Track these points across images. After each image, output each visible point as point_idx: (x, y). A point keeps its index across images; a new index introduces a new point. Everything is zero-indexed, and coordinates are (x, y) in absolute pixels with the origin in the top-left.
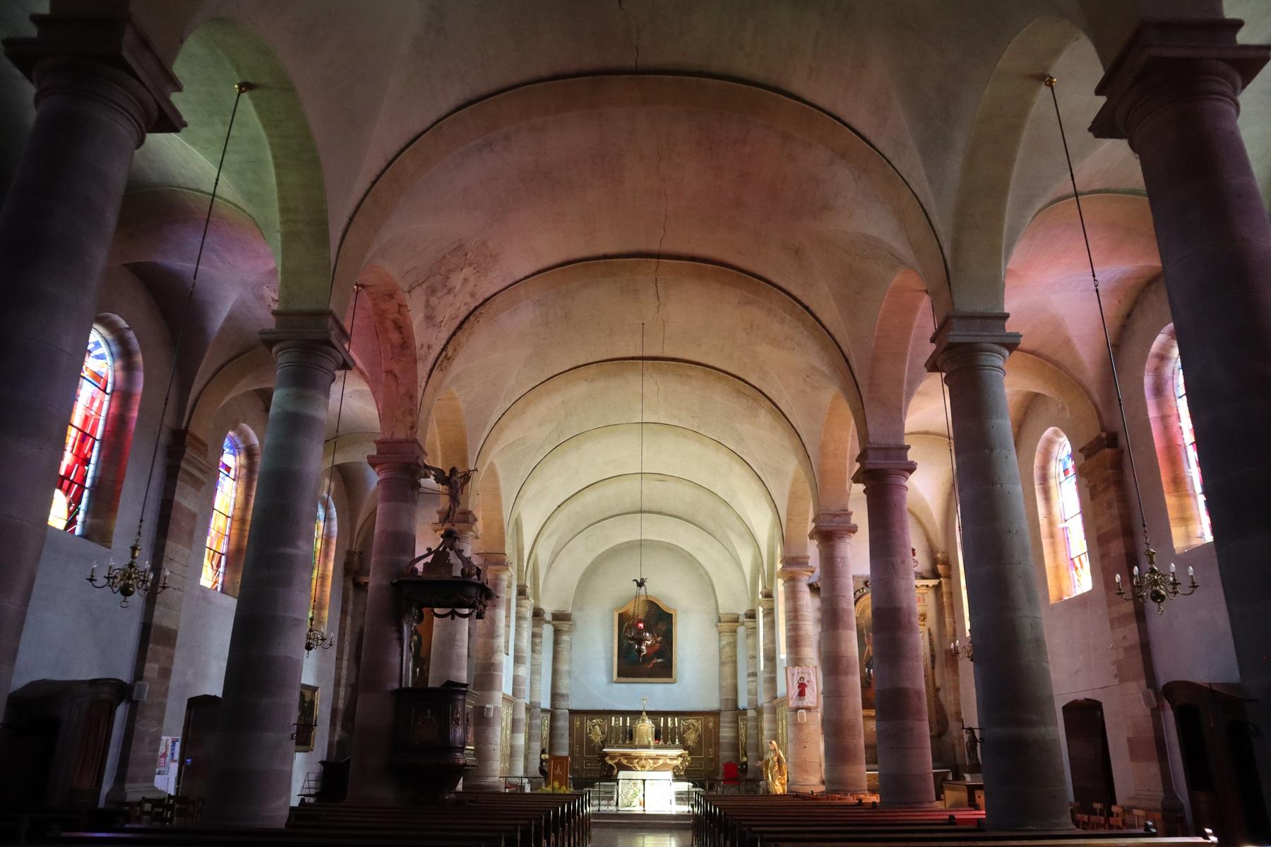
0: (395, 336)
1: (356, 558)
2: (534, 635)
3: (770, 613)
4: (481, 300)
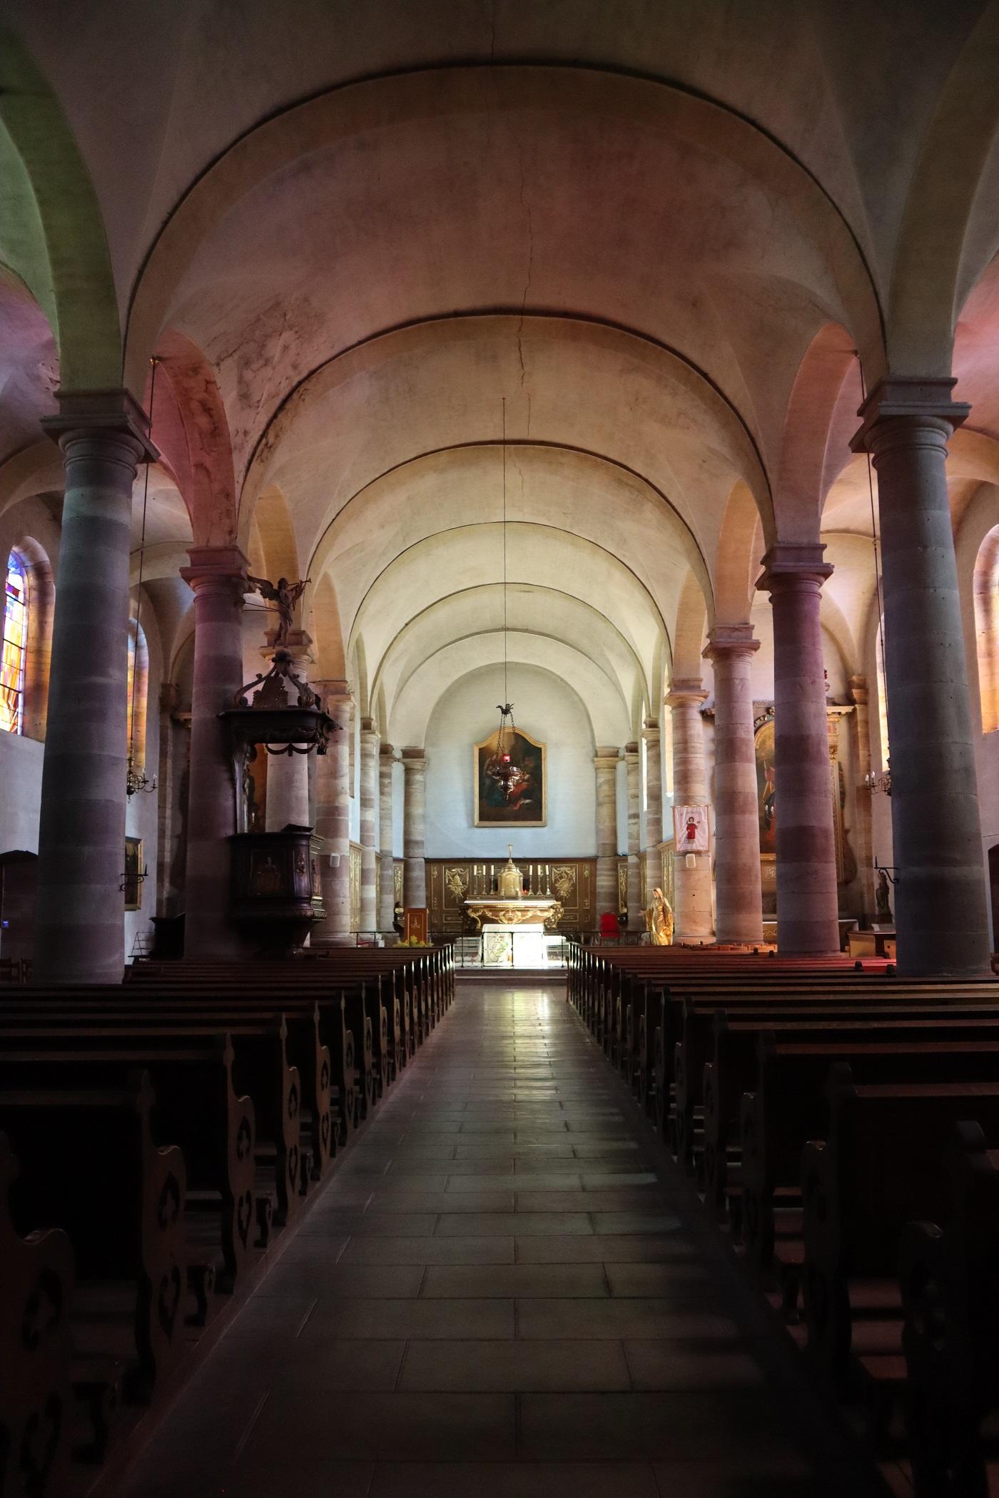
0: (203, 421)
1: (173, 692)
2: (382, 775)
3: (655, 745)
4: (305, 374)
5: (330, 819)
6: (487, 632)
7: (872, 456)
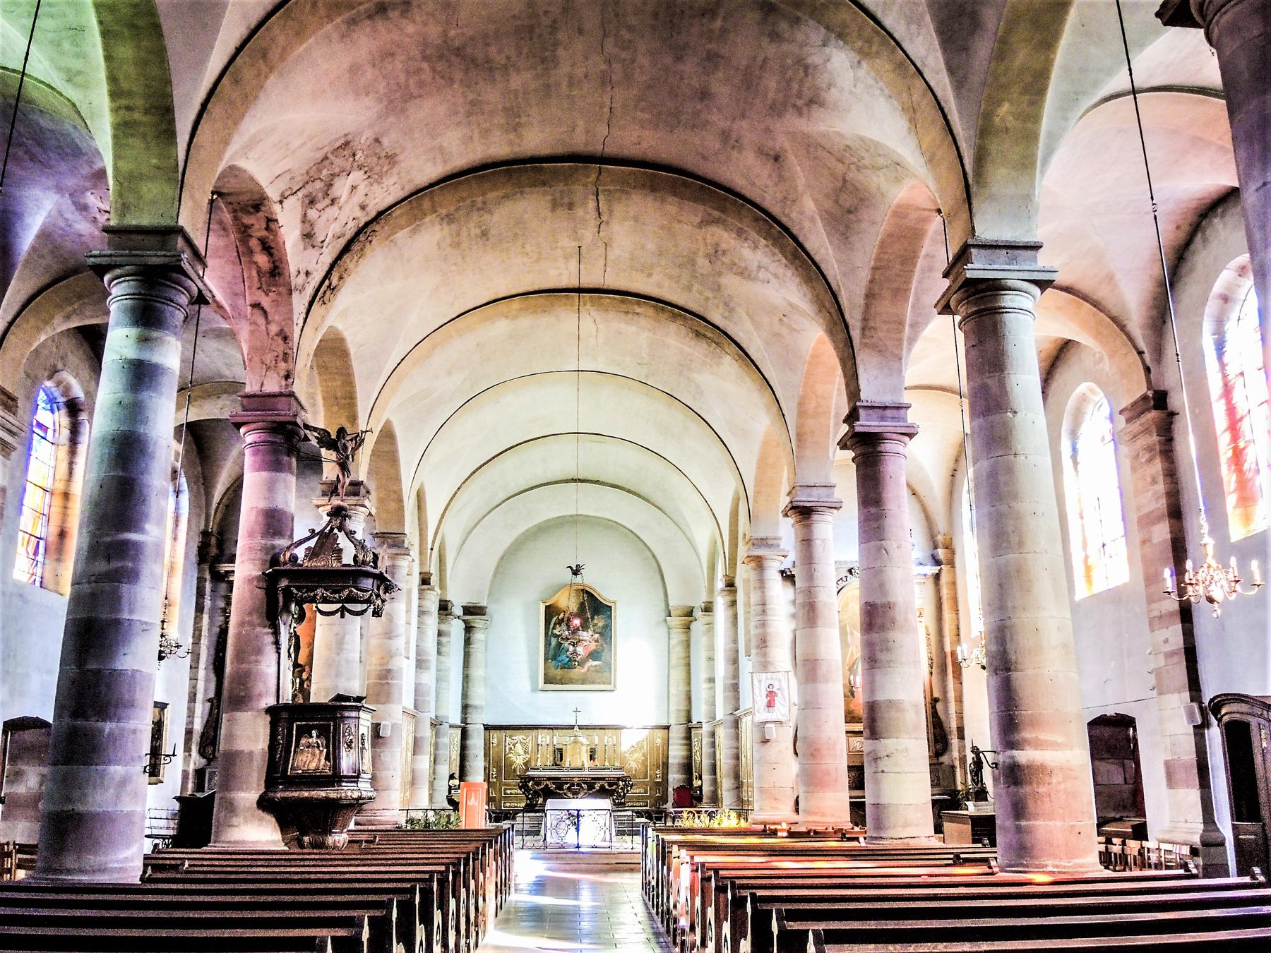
0: (262, 259)
1: (213, 541)
4: (373, 214)
5: (384, 680)
6: (557, 482)
7: (958, 318)
